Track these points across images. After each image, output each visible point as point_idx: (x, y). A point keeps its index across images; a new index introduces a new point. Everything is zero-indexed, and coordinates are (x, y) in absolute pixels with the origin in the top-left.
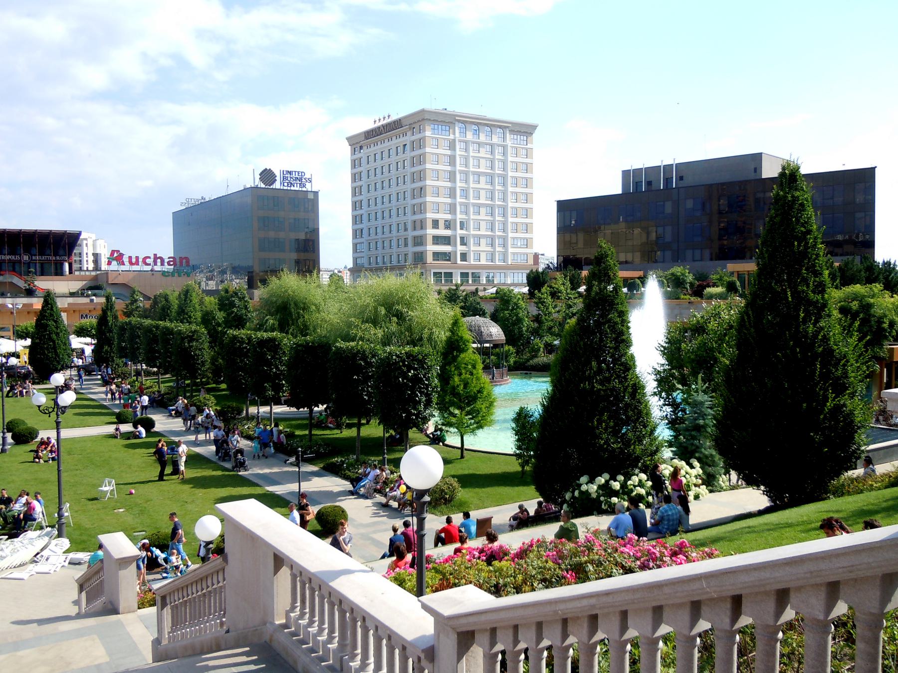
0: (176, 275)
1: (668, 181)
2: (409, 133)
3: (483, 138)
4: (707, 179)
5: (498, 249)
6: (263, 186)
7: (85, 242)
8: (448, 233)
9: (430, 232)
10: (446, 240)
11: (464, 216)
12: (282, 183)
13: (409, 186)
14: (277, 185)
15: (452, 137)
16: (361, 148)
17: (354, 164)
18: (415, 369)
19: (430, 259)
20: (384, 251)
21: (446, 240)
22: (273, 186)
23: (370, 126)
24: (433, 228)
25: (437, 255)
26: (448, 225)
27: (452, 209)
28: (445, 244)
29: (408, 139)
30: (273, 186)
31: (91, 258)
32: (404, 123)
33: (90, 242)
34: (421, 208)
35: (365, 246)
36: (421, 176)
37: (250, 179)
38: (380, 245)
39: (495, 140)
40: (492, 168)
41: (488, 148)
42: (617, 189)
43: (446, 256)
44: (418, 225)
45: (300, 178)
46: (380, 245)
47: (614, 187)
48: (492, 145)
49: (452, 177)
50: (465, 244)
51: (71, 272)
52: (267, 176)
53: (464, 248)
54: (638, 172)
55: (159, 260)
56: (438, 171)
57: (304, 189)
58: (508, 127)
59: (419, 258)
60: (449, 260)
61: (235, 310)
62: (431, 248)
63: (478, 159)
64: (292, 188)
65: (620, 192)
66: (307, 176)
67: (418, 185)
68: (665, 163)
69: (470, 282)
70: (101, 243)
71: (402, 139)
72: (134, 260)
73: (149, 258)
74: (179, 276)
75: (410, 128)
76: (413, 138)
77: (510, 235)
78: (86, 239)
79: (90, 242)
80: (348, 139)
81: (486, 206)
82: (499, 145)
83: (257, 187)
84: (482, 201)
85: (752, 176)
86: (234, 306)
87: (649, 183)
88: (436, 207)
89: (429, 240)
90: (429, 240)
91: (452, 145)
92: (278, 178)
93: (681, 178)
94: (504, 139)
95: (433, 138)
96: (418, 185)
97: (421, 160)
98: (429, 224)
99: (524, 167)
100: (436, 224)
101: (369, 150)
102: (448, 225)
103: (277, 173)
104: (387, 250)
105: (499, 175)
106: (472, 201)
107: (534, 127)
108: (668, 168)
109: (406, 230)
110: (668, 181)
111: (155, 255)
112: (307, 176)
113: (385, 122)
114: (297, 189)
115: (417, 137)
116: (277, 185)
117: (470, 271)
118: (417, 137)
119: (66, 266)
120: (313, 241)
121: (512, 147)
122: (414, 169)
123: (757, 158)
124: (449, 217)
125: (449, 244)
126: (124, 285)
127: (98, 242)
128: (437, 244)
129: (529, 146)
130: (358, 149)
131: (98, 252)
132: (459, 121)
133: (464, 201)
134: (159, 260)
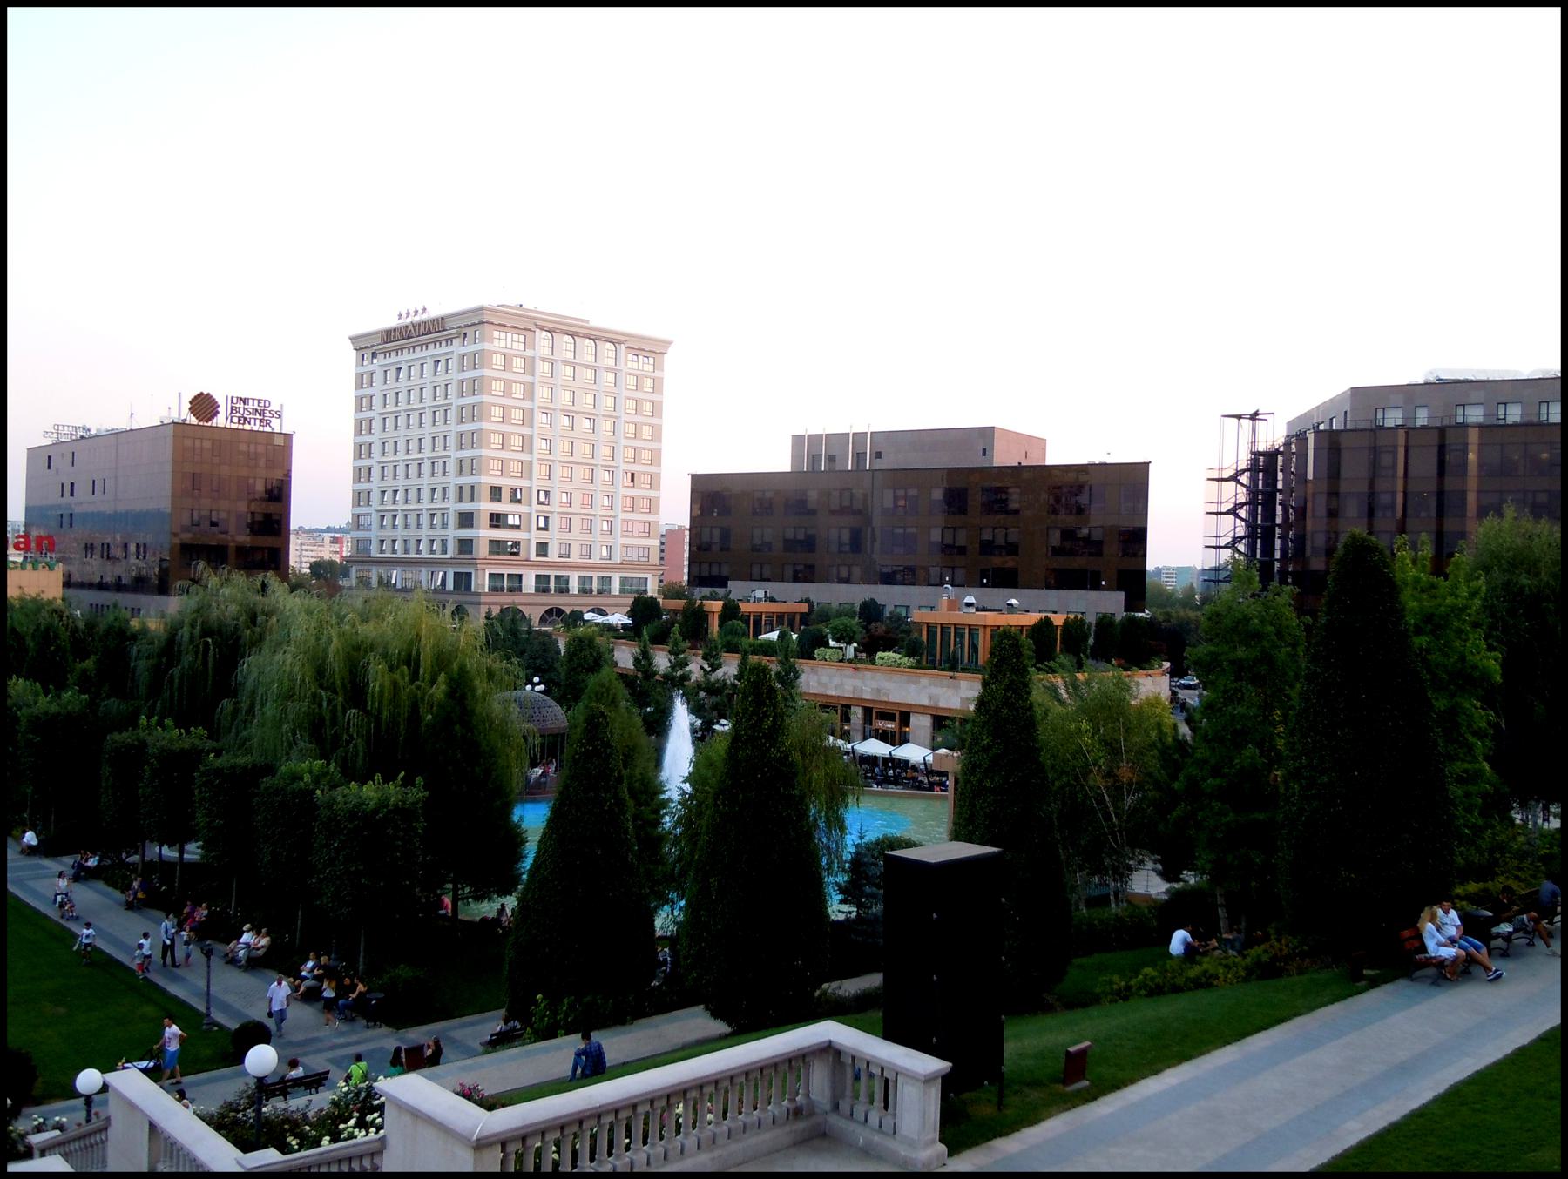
0: (29, 567)
4: (916, 461)
6: (194, 421)
12: (229, 418)
14: (220, 421)
16: (374, 355)
20: (408, 482)
22: (214, 423)
23: (392, 322)
27: (526, 470)
29: (457, 348)
30: (214, 423)
36: (474, 413)
37: (163, 405)
38: (401, 470)
44: (466, 493)
46: (401, 470)
52: (203, 405)
54: (814, 439)
57: (268, 429)
64: (247, 427)
65: (788, 468)
66: (275, 407)
74: (35, 569)
76: (463, 350)
83: (183, 424)
85: (978, 462)
87: (832, 459)
92: (222, 410)
93: (879, 455)
104: (412, 531)
107: (668, 343)
108: (859, 437)
109: (444, 525)
110: (859, 457)
112: (275, 407)
114: (256, 428)
115: (469, 348)
116: (220, 421)
117: (553, 573)
118: (469, 348)
120: (279, 522)
122: (461, 454)
123: (987, 433)
130: (368, 356)
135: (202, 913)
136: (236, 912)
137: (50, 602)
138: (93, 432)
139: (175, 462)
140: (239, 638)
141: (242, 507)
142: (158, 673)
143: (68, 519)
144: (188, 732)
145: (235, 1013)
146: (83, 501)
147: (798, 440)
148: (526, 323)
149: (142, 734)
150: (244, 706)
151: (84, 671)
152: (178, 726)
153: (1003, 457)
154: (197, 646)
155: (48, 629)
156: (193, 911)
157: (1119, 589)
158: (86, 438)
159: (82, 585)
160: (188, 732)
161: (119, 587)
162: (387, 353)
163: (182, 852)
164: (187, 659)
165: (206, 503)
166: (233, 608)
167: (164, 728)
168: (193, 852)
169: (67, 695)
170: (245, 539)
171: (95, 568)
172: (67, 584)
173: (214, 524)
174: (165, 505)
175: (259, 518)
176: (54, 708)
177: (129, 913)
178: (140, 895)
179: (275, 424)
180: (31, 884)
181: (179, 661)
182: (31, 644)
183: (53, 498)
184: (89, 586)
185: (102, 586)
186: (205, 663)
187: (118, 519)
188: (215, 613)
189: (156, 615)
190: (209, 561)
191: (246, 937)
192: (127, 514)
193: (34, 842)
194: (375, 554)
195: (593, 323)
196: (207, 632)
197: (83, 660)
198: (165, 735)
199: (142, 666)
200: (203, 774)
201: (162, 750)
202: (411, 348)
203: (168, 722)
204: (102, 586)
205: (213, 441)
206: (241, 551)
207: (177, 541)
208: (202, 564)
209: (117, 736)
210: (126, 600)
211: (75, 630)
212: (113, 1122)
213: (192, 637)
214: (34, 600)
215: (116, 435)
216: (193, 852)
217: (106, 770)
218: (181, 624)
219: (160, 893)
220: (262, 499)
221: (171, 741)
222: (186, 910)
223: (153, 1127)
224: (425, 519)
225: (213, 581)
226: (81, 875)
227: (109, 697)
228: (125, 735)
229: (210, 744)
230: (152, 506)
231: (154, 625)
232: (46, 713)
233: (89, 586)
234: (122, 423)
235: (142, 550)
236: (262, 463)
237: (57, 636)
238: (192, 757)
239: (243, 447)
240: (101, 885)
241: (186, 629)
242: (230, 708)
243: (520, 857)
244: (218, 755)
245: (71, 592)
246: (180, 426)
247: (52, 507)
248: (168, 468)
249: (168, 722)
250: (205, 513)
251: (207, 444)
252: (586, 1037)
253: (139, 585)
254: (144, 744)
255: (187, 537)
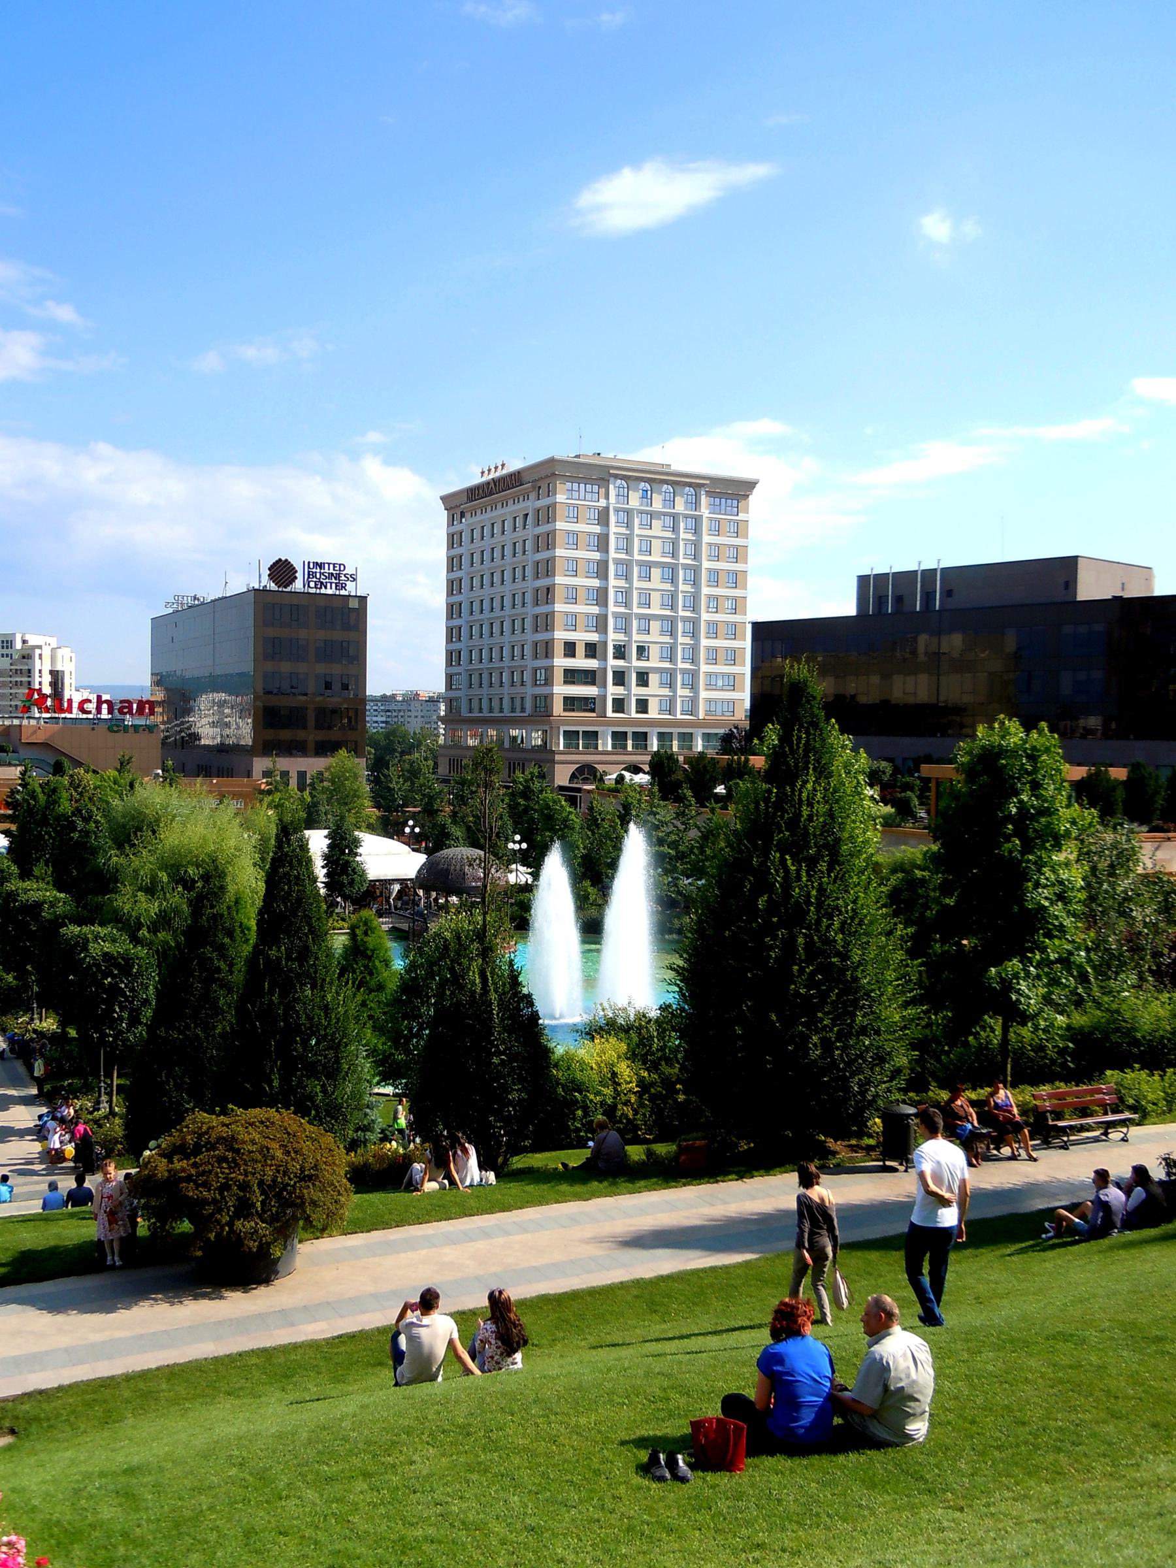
1: (928, 596)
2: (532, 496)
3: (657, 504)
5: (680, 692)
7: (38, 652)
8: (593, 664)
9: (561, 662)
10: (589, 677)
11: (621, 637)
13: (531, 584)
14: (298, 585)
15: (603, 503)
16: (462, 515)
17: (453, 540)
18: (114, 977)
19: (558, 708)
21: (589, 677)
23: (476, 479)
24: (566, 655)
25: (571, 703)
26: (592, 650)
27: (601, 624)
28: (586, 683)
29: (531, 504)
31: (47, 679)
32: (526, 478)
33: (46, 652)
34: (546, 622)
35: (464, 678)
36: (547, 568)
37: (246, 576)
39: (680, 507)
40: (674, 555)
41: (668, 521)
42: (849, 608)
43: (586, 704)
45: (338, 575)
47: (845, 606)
48: (675, 517)
49: (601, 570)
50: (623, 684)
52: (282, 571)
53: (620, 690)
54: (881, 578)
55: (105, 706)
56: (576, 560)
57: (343, 592)
58: (703, 485)
59: (543, 705)
60: (593, 710)
61: (76, 835)
62: (561, 690)
63: (648, 540)
64: (323, 591)
66: (349, 570)
67: (543, 582)
68: (926, 566)
69: (630, 748)
70: (64, 653)
71: (522, 505)
73: (90, 701)
75: (533, 487)
77: (704, 668)
78: (40, 647)
79: (46, 652)
80: (442, 498)
81: (661, 618)
82: (686, 517)
83: (264, 590)
84: (655, 610)
86: (74, 829)
87: (899, 599)
88: (572, 617)
89: (559, 676)
90: (559, 676)
91: (603, 517)
92: (299, 575)
94: (697, 505)
95: (569, 505)
96: (543, 582)
97: (547, 541)
98: (559, 649)
99: (733, 552)
100: (570, 649)
101: (474, 519)
102: (592, 650)
103: (298, 567)
105: (686, 567)
106: (636, 610)
107: (750, 485)
108: (929, 574)
110: (928, 596)
111: (99, 697)
112: (349, 570)
113: (498, 474)
114: (329, 591)
117: (630, 730)
121: (711, 519)
123: (1068, 565)
124: (594, 637)
125: (593, 683)
126: (45, 745)
127: (60, 652)
128: (573, 683)
129: (742, 516)
131: (59, 668)
132: (616, 477)
133: (622, 610)
134: (105, 706)
147: (863, 581)
148: (597, 475)
153: (1089, 589)
157: (159, 680)
162: (473, 513)
179: (350, 586)
194: (465, 713)
195: (676, 467)
202: (494, 507)
224: (527, 677)
246: (259, 594)
252: (807, 1181)
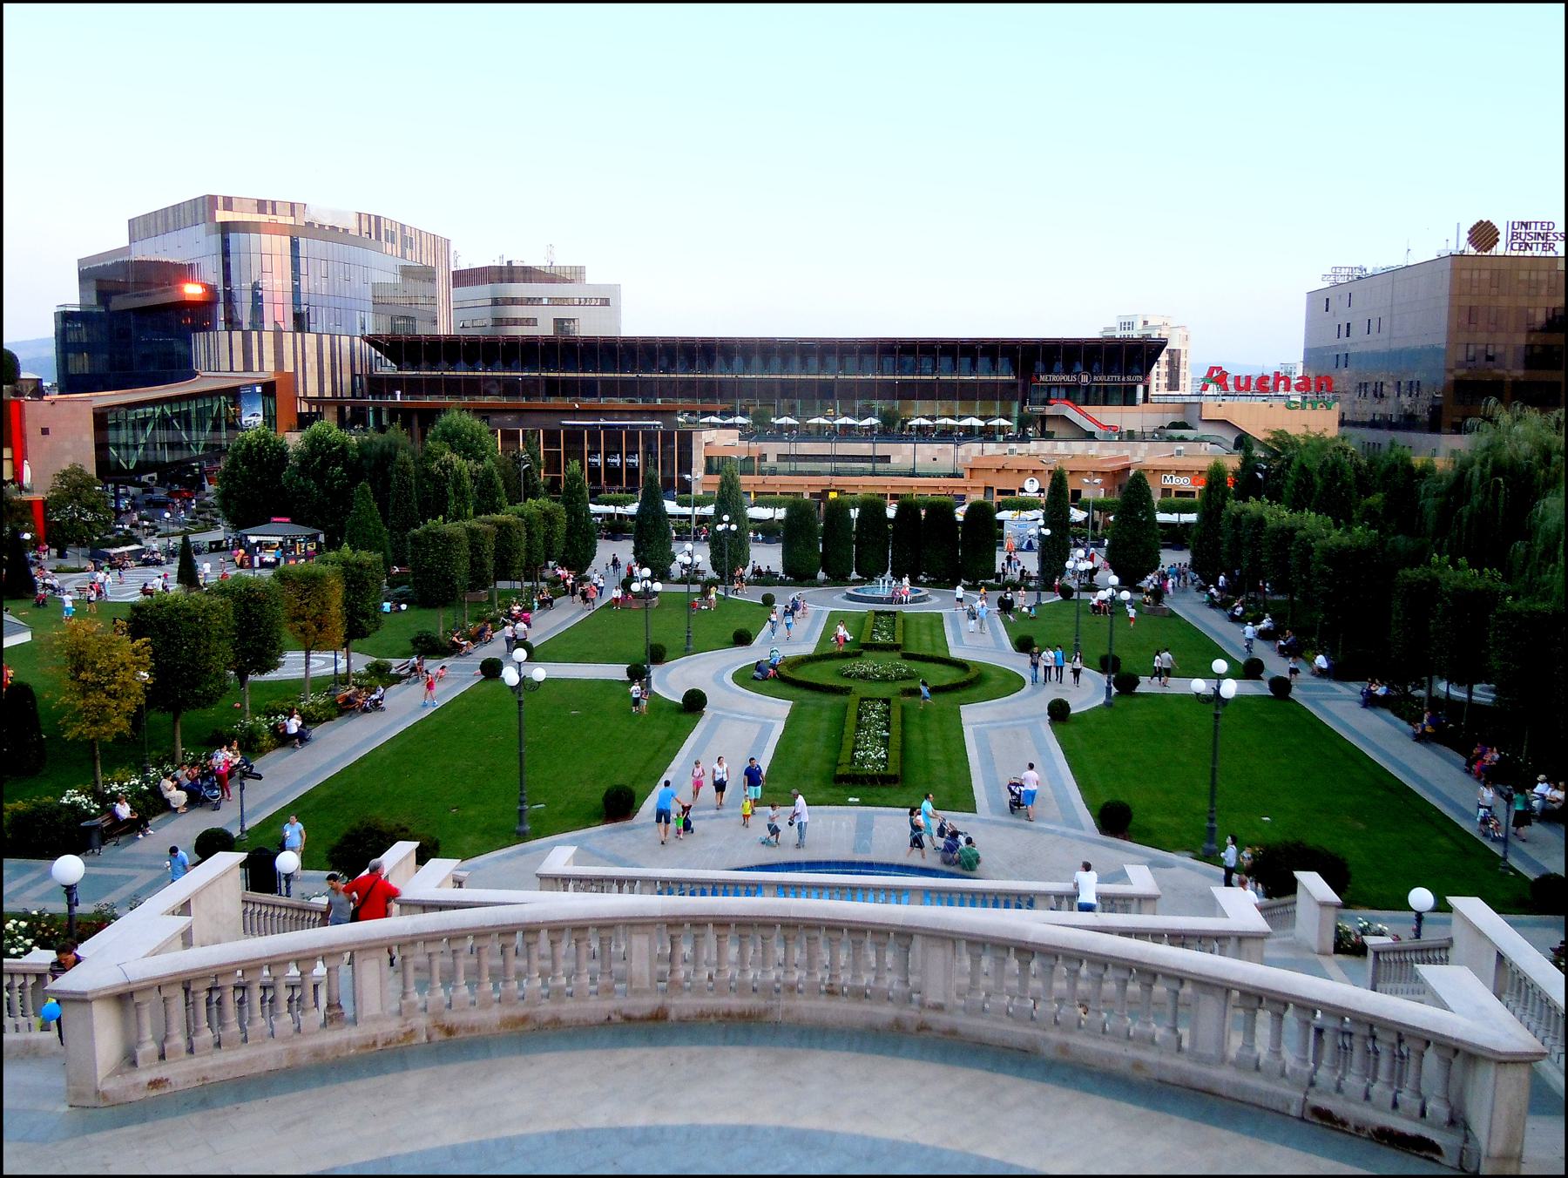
0: (1308, 406)
6: (1472, 251)
14: (1500, 249)
22: (1493, 252)
30: (1493, 252)
37: (1441, 237)
51: (1146, 400)
52: (1483, 234)
57: (1551, 253)
64: (1528, 253)
72: (1242, 384)
103: (1501, 228)
114: (1537, 254)
119: (1140, 388)
135: (1493, 756)
136: (1527, 760)
137: (1333, 440)
138: (1369, 271)
139: (1452, 296)
140: (1533, 477)
141: (1521, 339)
142: (1447, 512)
143: (1345, 360)
144: (1481, 573)
145: (1532, 863)
146: (1359, 342)
149: (1434, 572)
150: (1539, 548)
151: (1369, 507)
152: (1471, 565)
154: (1488, 486)
155: (1335, 466)
156: (1484, 753)
158: (1361, 279)
159: (1355, 424)
160: (1481, 573)
161: (1390, 425)
163: (1470, 693)
164: (1477, 499)
165: (1482, 337)
166: (1526, 447)
167: (1457, 567)
168: (1483, 694)
169: (1358, 530)
170: (1519, 373)
171: (1369, 408)
172: (1342, 423)
173: (1490, 358)
174: (1441, 341)
175: (1537, 350)
176: (1346, 540)
177: (1417, 745)
178: (1428, 729)
180: (1323, 703)
181: (1468, 501)
182: (1318, 480)
183: (1329, 339)
184: (1363, 424)
185: (1374, 425)
186: (1495, 504)
187: (1394, 357)
188: (1507, 451)
189: (1441, 453)
190: (1501, 400)
191: (1541, 788)
192: (1401, 351)
193: (1325, 666)
196: (1498, 469)
197: (1367, 496)
198: (1458, 575)
199: (1430, 504)
200: (1499, 617)
201: (1456, 589)
203: (1462, 561)
204: (1374, 425)
205: (1492, 271)
206: (1516, 384)
207: (1451, 378)
208: (1493, 401)
209: (1408, 572)
210: (1400, 437)
211: (1358, 468)
212: (1456, 942)
213: (1482, 477)
214: (1318, 438)
215: (1392, 273)
216: (1483, 694)
217: (1397, 604)
218: (1472, 463)
219: (1449, 730)
220: (1542, 330)
221: (1464, 580)
222: (1476, 751)
223: (1501, 957)
225: (1505, 418)
226: (1370, 701)
227: (1395, 533)
228: (1417, 571)
229: (1503, 587)
230: (1427, 342)
231: (1441, 463)
232: (1339, 546)
233: (1363, 424)
234: (1397, 260)
235: (1414, 388)
236: (1544, 291)
237: (1343, 472)
238: (1485, 600)
239: (1523, 275)
240: (1388, 714)
241: (1477, 467)
242: (1523, 550)
243: (262, 672)
244: (1516, 598)
245: (1348, 430)
247: (1329, 348)
248: (1445, 302)
249: (1462, 561)
250: (1482, 347)
251: (1486, 275)
253: (1408, 422)
254: (1436, 581)
255: (1462, 372)
